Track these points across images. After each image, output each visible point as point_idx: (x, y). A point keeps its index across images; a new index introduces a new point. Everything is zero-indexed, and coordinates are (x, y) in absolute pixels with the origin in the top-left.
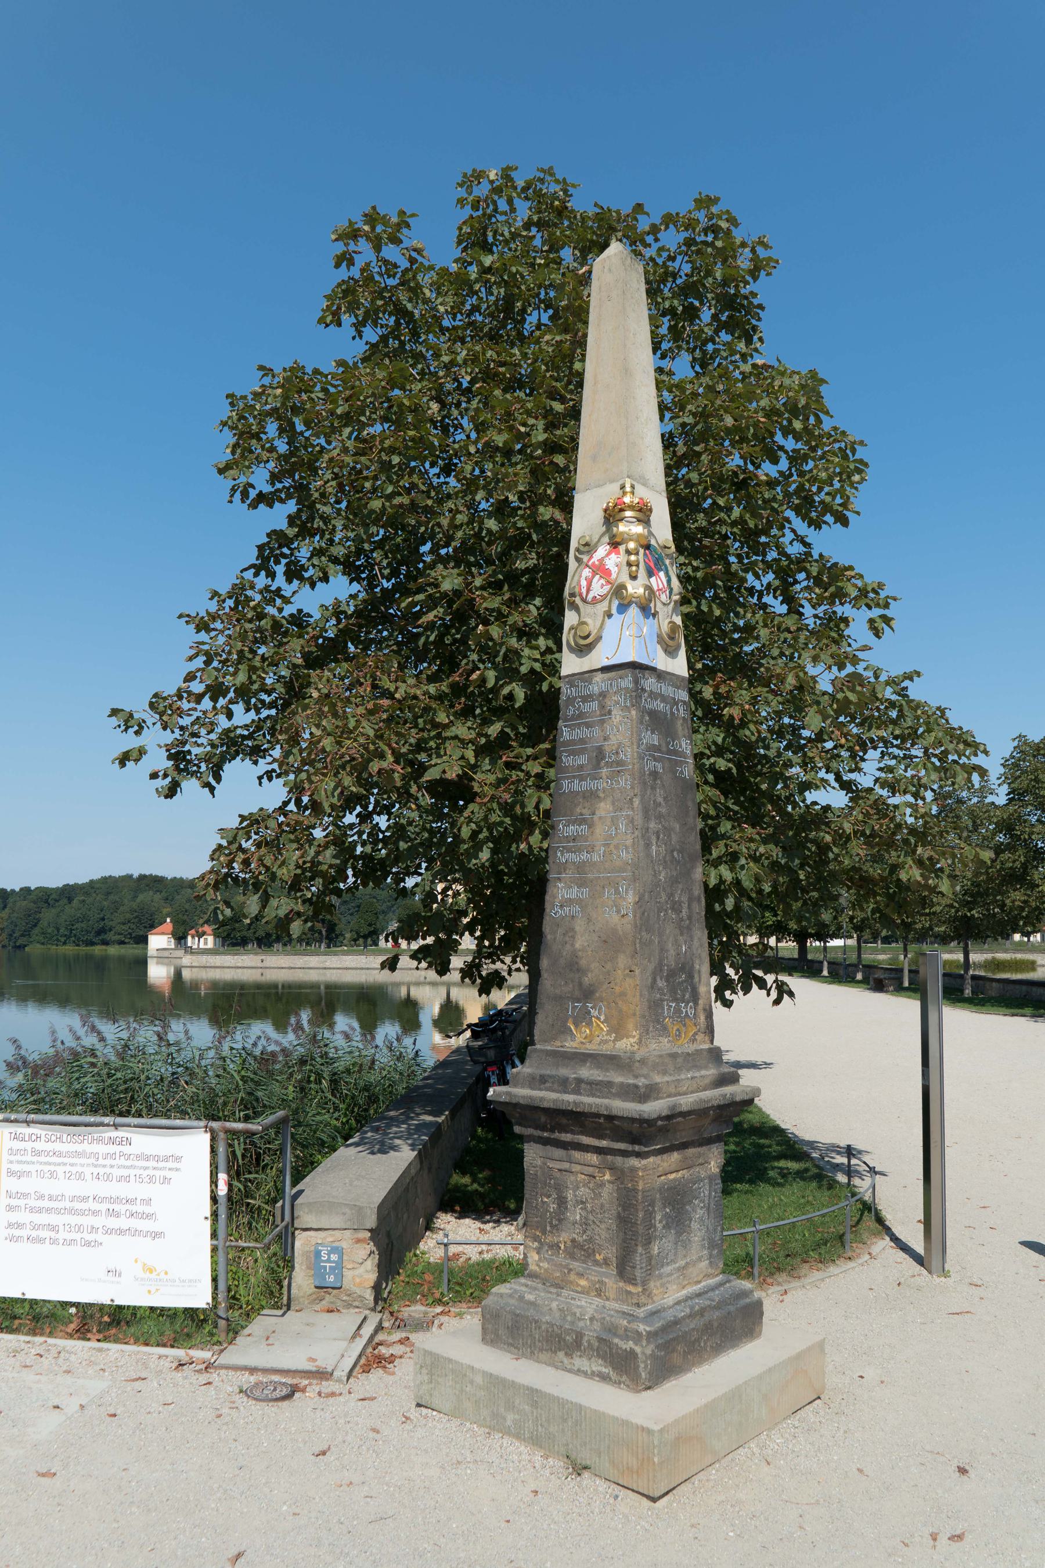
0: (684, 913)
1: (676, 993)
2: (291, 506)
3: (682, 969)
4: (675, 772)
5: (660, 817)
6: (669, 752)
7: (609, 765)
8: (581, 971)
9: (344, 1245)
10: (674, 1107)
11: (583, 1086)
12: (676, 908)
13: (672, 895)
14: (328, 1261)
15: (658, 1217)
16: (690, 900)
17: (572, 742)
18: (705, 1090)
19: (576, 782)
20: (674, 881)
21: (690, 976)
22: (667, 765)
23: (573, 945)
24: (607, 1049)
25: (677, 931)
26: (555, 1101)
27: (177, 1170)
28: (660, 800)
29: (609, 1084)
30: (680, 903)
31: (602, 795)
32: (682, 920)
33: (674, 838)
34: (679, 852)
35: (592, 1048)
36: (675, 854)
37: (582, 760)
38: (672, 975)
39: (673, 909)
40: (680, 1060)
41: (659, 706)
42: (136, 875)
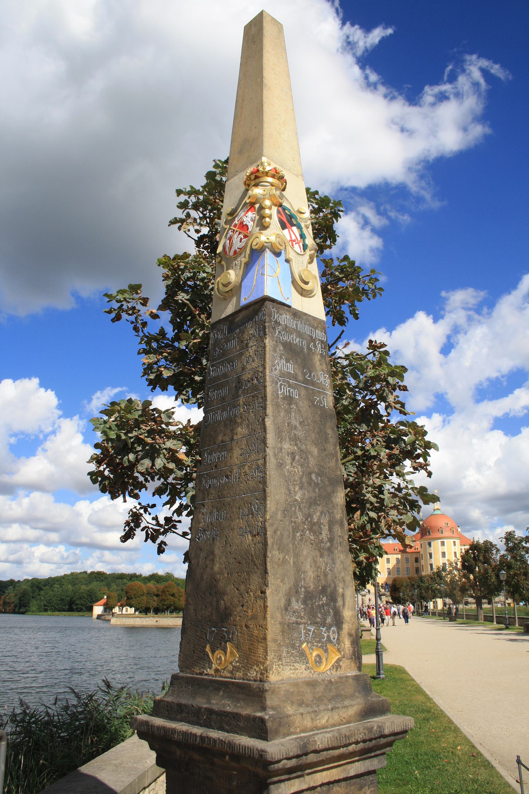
0: (325, 534)
1: (315, 616)
3: (323, 591)
4: (312, 401)
5: (295, 440)
6: (306, 381)
7: (246, 392)
8: (220, 594)
11: (214, 716)
12: (315, 528)
13: (310, 515)
16: (331, 523)
17: (217, 378)
18: (349, 722)
19: (219, 412)
20: (312, 503)
21: (333, 598)
22: (303, 392)
23: (212, 568)
24: (239, 678)
25: (317, 553)
26: (185, 734)
28: (294, 422)
29: (236, 716)
30: (319, 524)
31: (239, 421)
32: (322, 541)
33: (312, 462)
34: (318, 475)
35: (225, 676)
36: (313, 476)
37: (224, 392)
38: (309, 597)
39: (311, 530)
40: (320, 689)
42: (89, 571)
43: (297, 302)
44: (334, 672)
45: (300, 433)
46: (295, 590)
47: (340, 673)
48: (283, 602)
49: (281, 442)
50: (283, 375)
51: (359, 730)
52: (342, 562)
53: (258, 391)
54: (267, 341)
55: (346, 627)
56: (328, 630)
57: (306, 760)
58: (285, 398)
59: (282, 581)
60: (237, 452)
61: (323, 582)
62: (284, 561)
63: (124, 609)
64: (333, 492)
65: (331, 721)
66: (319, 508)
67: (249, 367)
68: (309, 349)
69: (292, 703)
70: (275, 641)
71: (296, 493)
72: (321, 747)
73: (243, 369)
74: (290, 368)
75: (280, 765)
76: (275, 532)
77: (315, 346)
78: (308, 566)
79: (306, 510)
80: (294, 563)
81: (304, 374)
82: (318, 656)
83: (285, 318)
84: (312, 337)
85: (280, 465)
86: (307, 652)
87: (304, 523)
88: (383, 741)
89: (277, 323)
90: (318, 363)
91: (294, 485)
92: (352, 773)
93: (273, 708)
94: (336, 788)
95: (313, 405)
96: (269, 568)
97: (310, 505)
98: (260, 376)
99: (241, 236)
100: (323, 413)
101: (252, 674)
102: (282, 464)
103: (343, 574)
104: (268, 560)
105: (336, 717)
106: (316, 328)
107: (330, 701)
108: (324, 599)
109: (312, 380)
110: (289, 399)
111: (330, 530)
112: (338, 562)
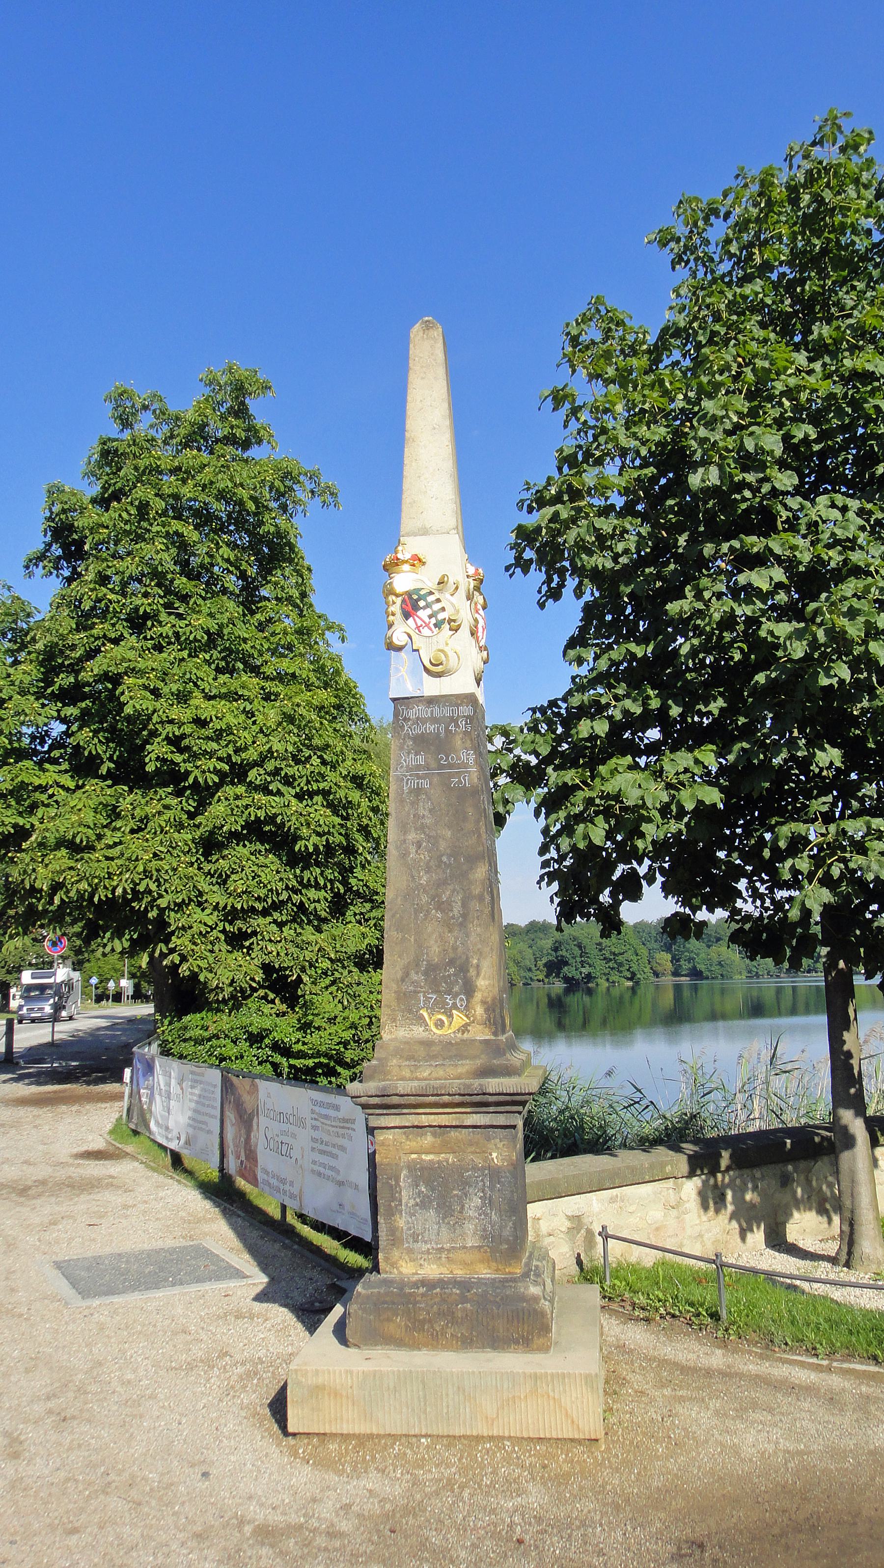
0: (457, 909)
3: (452, 962)
5: (422, 828)
12: (441, 906)
13: (438, 896)
20: (442, 884)
21: (463, 969)
28: (421, 812)
30: (449, 903)
36: (445, 859)
38: (431, 970)
41: (431, 728)
44: (459, 1035)
45: (428, 821)
48: (399, 975)
50: (409, 769)
52: (479, 935)
55: (478, 996)
56: (455, 997)
58: (411, 791)
61: (452, 955)
62: (404, 939)
64: (471, 869)
65: (434, 1075)
66: (451, 887)
71: (420, 878)
74: (421, 760)
76: (393, 916)
77: (457, 726)
78: (432, 942)
79: (432, 892)
80: (415, 940)
85: (404, 855)
92: (468, 1122)
94: (453, 1133)
97: (439, 886)
103: (480, 946)
105: (441, 1073)
106: (458, 706)
110: (417, 791)
111: (464, 905)
112: (473, 938)
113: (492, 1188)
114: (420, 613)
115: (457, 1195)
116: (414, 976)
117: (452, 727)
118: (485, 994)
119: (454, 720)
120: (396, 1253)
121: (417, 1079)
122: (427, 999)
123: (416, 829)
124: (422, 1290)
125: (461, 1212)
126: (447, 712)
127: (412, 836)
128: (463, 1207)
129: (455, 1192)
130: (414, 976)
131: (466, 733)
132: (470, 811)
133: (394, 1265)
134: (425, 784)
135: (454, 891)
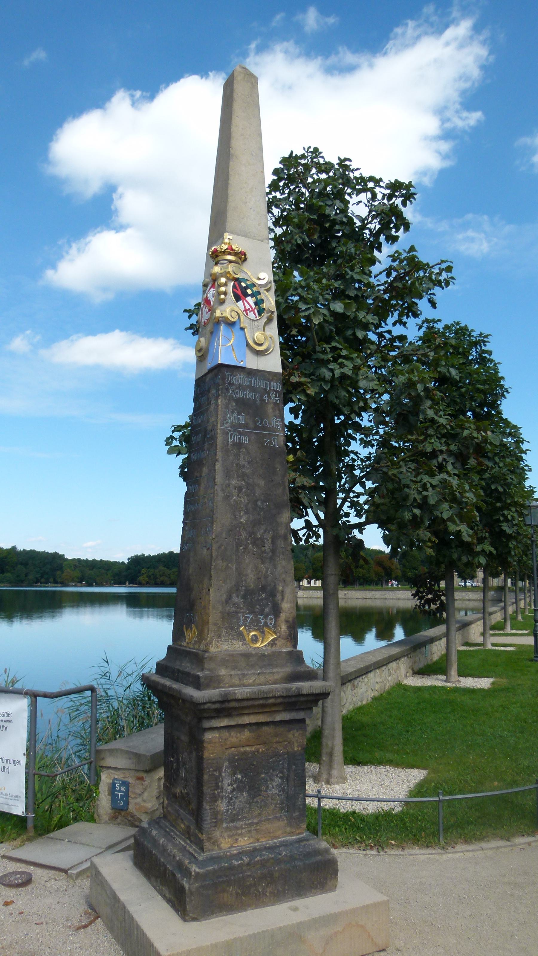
0: (268, 546)
2: (394, 344)
3: (263, 589)
5: (243, 476)
9: (130, 780)
10: (226, 695)
12: (258, 542)
14: (120, 791)
15: (227, 782)
21: (272, 594)
27: (10, 721)
28: (242, 462)
29: (188, 674)
30: (262, 539)
31: (204, 462)
32: (265, 552)
34: (263, 502)
36: (259, 503)
38: (248, 594)
39: (254, 544)
41: (250, 395)
43: (252, 362)
45: (248, 471)
46: (237, 588)
47: (274, 649)
48: (224, 597)
49: (229, 480)
50: (233, 426)
51: (280, 688)
52: (284, 567)
53: (214, 438)
54: (220, 401)
55: (283, 616)
56: (266, 617)
57: (226, 705)
59: (224, 582)
60: (203, 486)
62: (227, 567)
63: (313, 581)
64: (279, 513)
65: (257, 681)
66: (263, 527)
67: (211, 420)
68: (262, 400)
69: (227, 667)
70: (216, 624)
71: (241, 517)
72: (240, 697)
73: (208, 422)
74: (242, 419)
75: (206, 707)
76: (219, 547)
77: (269, 397)
78: (249, 571)
80: (236, 569)
81: (255, 423)
82: (255, 635)
83: (239, 379)
84: (266, 389)
85: (227, 497)
86: (245, 633)
87: (248, 539)
88: (302, 699)
89: (231, 384)
90: (271, 410)
91: (240, 511)
93: (209, 670)
94: (265, 729)
95: (264, 446)
96: (212, 573)
98: (214, 427)
99: (207, 309)
100: (273, 452)
101: (202, 647)
102: (229, 496)
103: (284, 576)
104: (213, 567)
106: (270, 381)
107: (261, 668)
108: (264, 595)
109: (263, 426)
111: (273, 542)
112: (279, 569)
113: (289, 770)
114: (249, 299)
115: (263, 778)
116: (235, 599)
117: (265, 397)
118: (288, 615)
119: (266, 391)
120: (217, 834)
121: (245, 686)
122: (246, 618)
123: (238, 476)
124: (246, 860)
125: (266, 791)
126: (262, 384)
127: (234, 482)
128: (267, 787)
129: (263, 776)
130: (235, 599)
131: (275, 403)
132: (278, 467)
133: (215, 843)
134: (245, 441)
135: (265, 531)
